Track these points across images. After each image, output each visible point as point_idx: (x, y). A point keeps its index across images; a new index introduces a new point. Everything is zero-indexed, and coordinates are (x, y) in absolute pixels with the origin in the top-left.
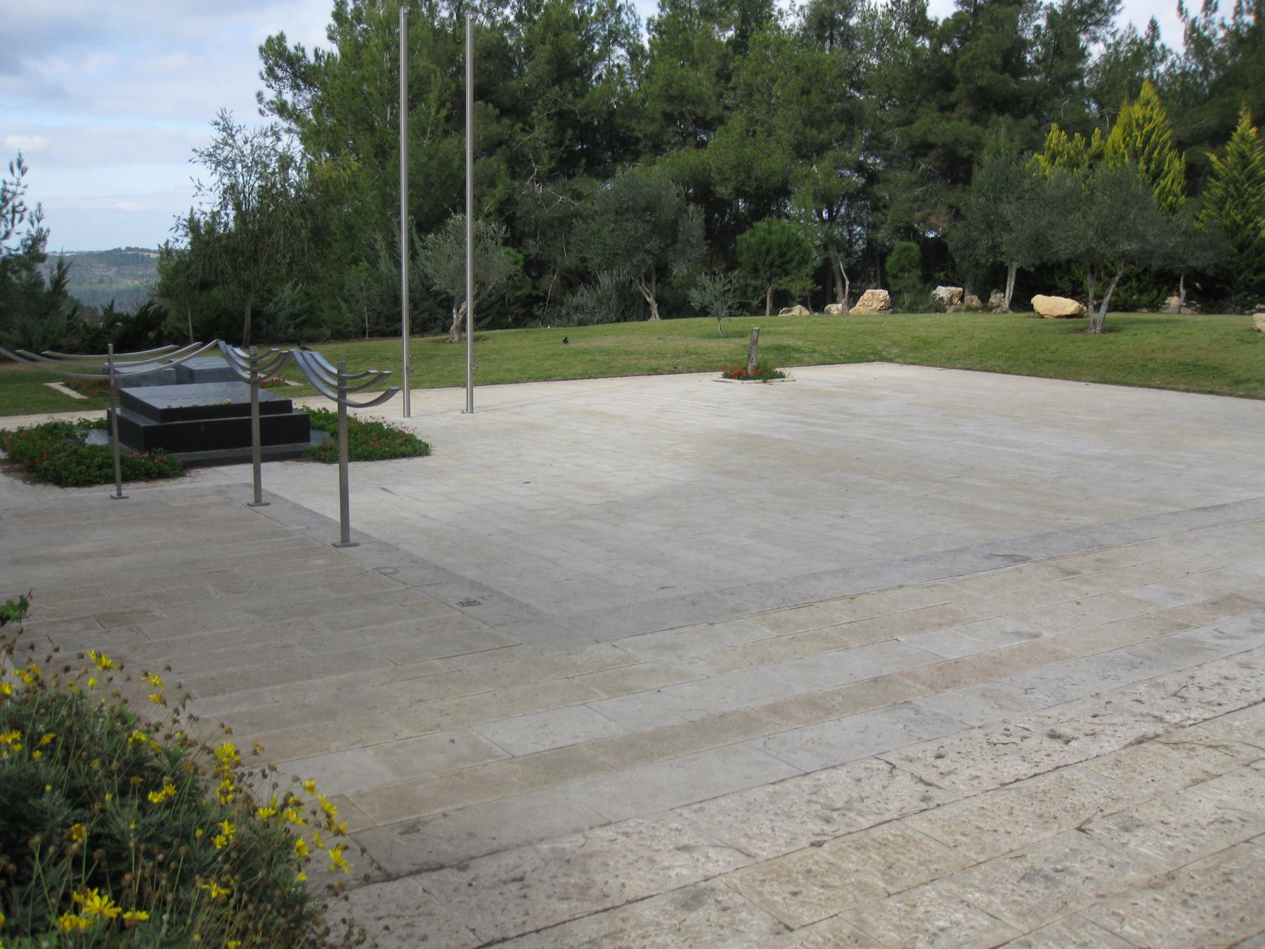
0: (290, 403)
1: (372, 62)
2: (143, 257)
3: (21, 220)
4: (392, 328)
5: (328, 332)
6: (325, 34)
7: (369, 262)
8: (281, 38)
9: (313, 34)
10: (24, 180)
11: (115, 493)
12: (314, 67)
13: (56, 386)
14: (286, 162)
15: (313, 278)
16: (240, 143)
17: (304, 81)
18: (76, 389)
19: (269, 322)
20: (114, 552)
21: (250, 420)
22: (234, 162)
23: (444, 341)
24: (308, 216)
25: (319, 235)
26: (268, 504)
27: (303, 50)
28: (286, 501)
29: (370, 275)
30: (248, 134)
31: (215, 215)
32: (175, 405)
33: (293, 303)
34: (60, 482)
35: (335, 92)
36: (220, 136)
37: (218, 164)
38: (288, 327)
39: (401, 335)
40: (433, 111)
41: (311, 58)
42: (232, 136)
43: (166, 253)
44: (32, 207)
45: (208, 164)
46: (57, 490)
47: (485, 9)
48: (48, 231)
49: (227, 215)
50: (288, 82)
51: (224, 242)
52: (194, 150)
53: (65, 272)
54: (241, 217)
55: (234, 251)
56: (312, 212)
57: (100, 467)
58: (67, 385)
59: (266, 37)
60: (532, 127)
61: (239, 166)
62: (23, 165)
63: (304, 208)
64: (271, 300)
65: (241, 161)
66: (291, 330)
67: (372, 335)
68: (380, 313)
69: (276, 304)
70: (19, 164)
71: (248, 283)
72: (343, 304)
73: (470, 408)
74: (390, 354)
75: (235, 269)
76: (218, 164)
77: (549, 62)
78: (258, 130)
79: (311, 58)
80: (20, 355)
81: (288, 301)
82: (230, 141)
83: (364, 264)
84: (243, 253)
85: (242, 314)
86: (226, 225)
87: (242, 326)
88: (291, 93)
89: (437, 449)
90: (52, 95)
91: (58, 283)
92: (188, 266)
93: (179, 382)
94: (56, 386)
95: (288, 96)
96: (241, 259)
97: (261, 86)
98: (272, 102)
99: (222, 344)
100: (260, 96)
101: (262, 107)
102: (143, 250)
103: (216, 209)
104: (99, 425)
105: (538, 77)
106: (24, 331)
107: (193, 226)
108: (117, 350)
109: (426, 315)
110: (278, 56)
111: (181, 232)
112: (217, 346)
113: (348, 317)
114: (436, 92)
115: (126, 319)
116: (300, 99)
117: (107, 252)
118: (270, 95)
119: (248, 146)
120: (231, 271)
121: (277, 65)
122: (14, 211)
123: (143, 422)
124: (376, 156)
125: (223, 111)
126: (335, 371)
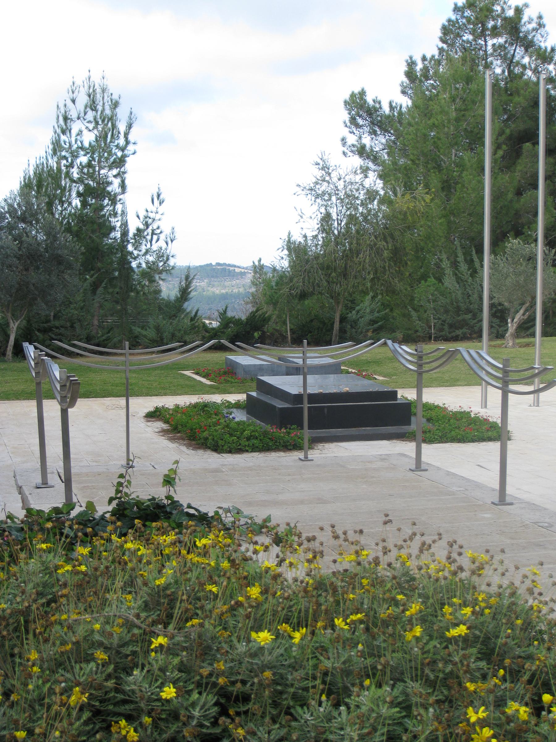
0: (395, 393)
1: (441, 112)
2: (230, 271)
3: (158, 240)
4: (453, 334)
6: (399, 89)
7: (435, 278)
8: (363, 93)
9: (389, 92)
10: (161, 209)
11: (302, 457)
12: (389, 116)
13: (188, 373)
14: (371, 195)
15: (391, 291)
16: (335, 179)
17: (380, 127)
20: (321, 501)
21: (302, 408)
24: (389, 239)
25: (397, 255)
26: (426, 470)
27: (380, 103)
28: (439, 469)
29: (437, 289)
33: (372, 311)
34: (217, 449)
35: (410, 137)
36: (320, 174)
38: (368, 331)
39: (480, 336)
41: (386, 109)
42: (329, 174)
44: (166, 228)
45: (309, 196)
46: (215, 455)
47: (533, 66)
50: (367, 129)
52: (299, 186)
53: (190, 283)
55: (328, 267)
56: (392, 236)
57: (248, 439)
58: (197, 374)
59: (350, 93)
61: (334, 198)
62: (161, 197)
63: (387, 234)
64: (353, 309)
67: (437, 339)
68: (444, 321)
69: (358, 312)
70: (159, 196)
72: (413, 313)
75: (328, 282)
78: (350, 168)
79: (386, 109)
80: (238, 347)
81: (368, 310)
82: (327, 178)
88: (369, 138)
91: (185, 293)
92: (291, 280)
93: (287, 374)
94: (188, 373)
95: (367, 140)
96: (334, 274)
97: (345, 132)
98: (353, 146)
99: (389, 342)
100: (343, 140)
101: (345, 149)
102: (229, 265)
104: (238, 405)
106: (158, 329)
108: (309, 344)
110: (360, 109)
112: (385, 344)
115: (238, 322)
116: (377, 143)
117: (201, 267)
118: (352, 139)
120: (325, 284)
122: (153, 234)
123: (280, 404)
124: (443, 189)
126: (501, 366)
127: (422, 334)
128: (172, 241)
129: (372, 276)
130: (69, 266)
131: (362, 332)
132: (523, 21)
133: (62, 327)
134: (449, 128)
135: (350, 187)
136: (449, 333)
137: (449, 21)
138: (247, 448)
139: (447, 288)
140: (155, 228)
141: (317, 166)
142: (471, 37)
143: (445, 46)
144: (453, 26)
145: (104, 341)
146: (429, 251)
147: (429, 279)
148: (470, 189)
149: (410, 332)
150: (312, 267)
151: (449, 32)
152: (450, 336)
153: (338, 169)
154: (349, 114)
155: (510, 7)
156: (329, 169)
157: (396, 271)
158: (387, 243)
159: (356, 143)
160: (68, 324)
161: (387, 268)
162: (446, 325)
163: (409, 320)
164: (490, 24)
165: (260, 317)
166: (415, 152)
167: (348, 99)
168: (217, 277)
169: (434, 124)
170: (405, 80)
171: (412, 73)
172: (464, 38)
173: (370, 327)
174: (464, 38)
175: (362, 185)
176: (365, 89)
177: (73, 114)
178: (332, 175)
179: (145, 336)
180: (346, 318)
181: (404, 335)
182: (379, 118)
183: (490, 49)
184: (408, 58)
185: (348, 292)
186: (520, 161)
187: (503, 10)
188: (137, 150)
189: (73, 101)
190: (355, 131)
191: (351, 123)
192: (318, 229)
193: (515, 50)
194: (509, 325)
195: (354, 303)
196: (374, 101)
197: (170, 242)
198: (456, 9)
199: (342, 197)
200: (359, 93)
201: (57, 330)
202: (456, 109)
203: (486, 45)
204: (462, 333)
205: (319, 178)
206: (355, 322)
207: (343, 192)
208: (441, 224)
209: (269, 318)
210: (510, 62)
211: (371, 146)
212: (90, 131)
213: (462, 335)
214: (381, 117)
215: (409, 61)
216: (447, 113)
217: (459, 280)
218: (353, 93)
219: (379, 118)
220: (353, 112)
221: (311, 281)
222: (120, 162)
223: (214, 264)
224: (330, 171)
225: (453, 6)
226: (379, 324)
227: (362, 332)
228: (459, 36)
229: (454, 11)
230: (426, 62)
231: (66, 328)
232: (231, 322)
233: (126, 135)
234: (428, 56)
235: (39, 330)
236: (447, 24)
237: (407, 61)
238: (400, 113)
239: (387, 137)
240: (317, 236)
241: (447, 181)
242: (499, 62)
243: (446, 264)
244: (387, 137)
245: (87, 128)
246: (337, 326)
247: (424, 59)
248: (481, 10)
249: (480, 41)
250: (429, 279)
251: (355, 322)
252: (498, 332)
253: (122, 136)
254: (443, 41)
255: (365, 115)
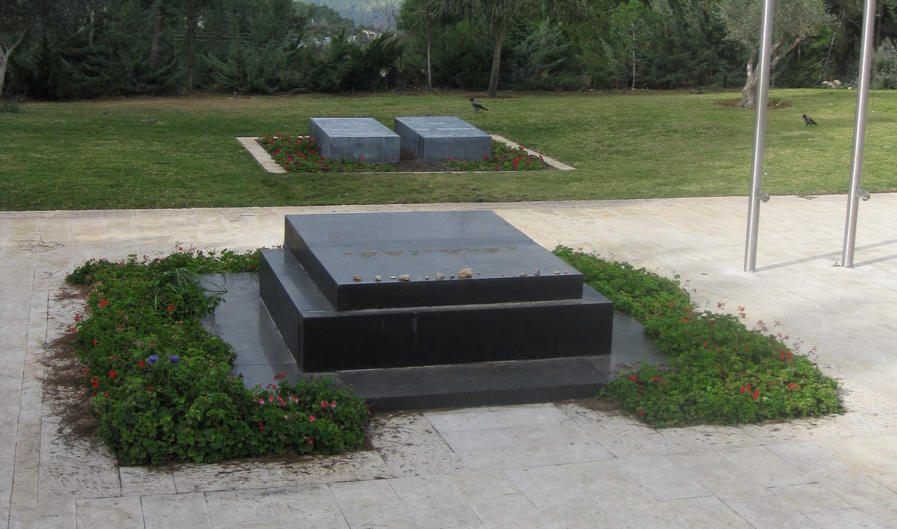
4: (663, 79)
5: (587, 79)
18: (273, 151)
19: (519, 64)
29: (642, 16)
32: (367, 279)
33: (549, 43)
38: (542, 71)
66: (545, 75)
67: (639, 86)
68: (651, 61)
69: (530, 43)
71: (500, 20)
72: (607, 48)
73: (849, 254)
74: (675, 124)
81: (543, 41)
85: (490, 54)
87: (489, 69)
89: (856, 391)
109: (704, 66)
113: (613, 64)
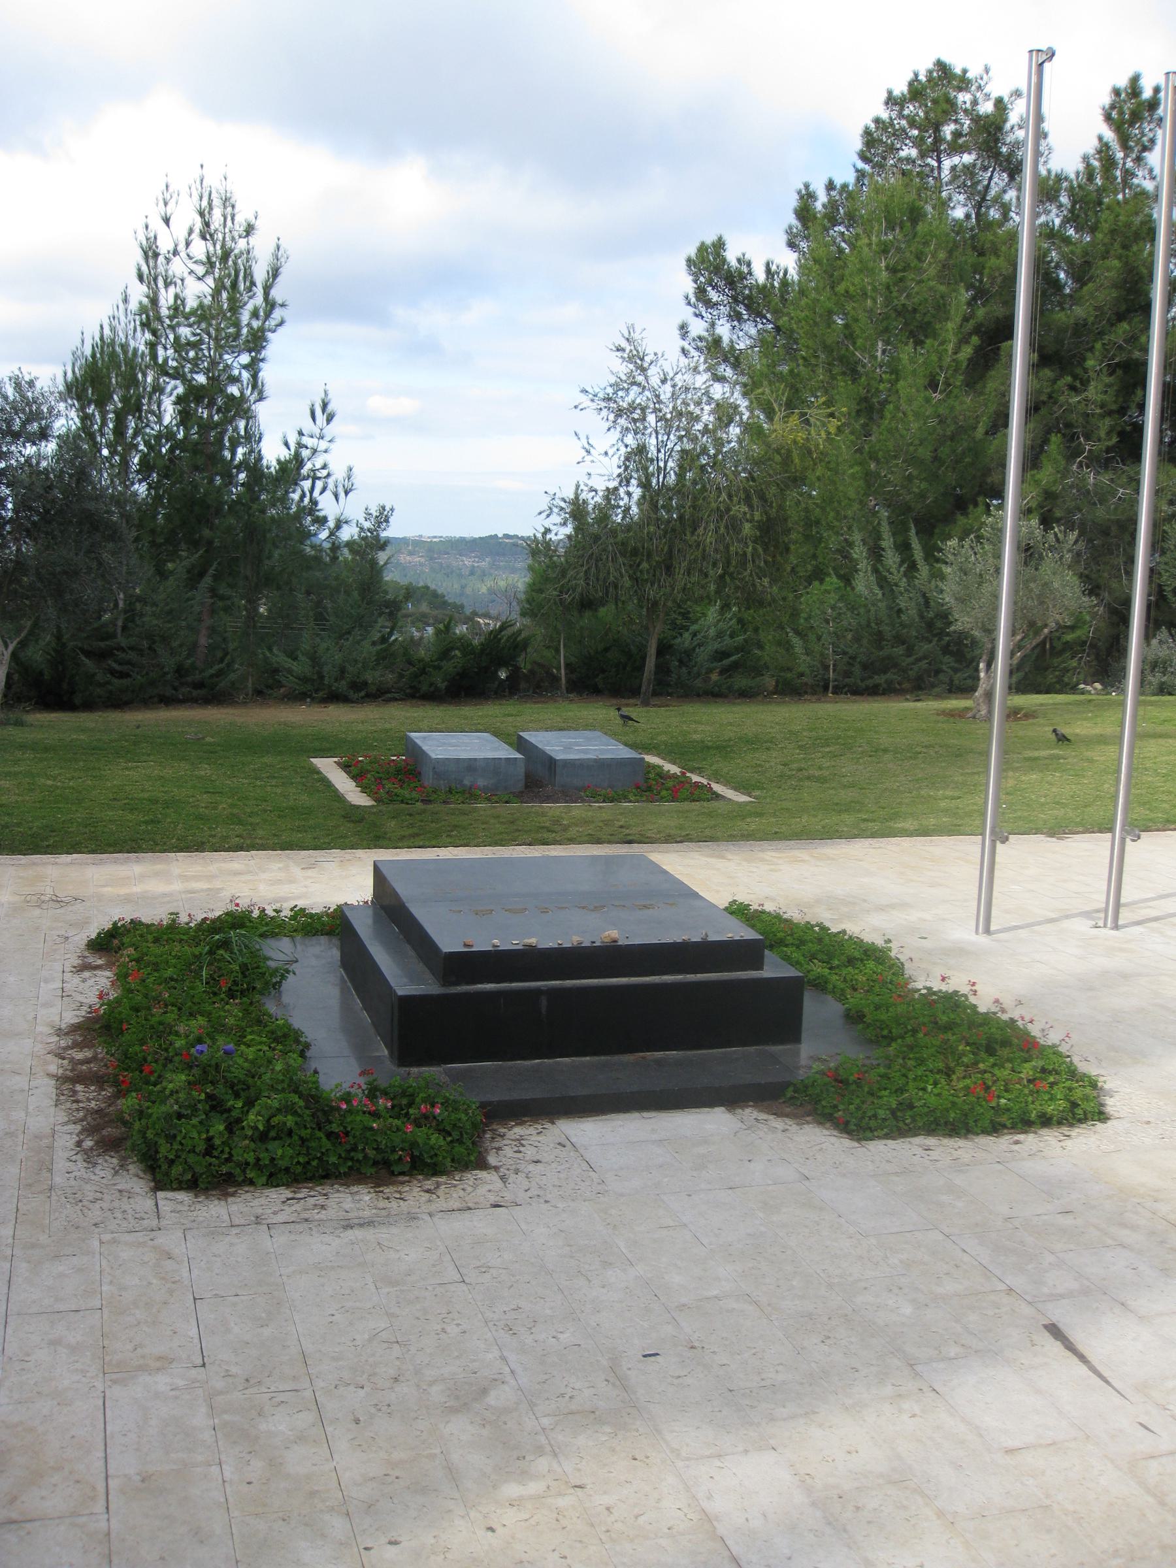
1: (860, 271)
4: (870, 682)
5: (769, 682)
6: (784, 238)
7: (839, 577)
9: (766, 248)
10: (330, 431)
15: (753, 600)
16: (655, 381)
17: (748, 308)
18: (358, 776)
22: (643, 409)
23: (960, 714)
24: (755, 501)
25: (770, 532)
27: (749, 264)
29: (841, 598)
30: (668, 369)
31: (611, 493)
33: (720, 635)
36: (623, 369)
37: (620, 412)
38: (710, 671)
40: (950, 347)
41: (760, 276)
42: (643, 370)
43: (539, 548)
44: (338, 472)
45: (605, 413)
48: (392, 510)
49: (629, 494)
50: (724, 310)
51: (621, 536)
52: (584, 391)
54: (651, 497)
55: (635, 552)
56: (763, 498)
60: (1085, 383)
61: (651, 419)
62: (330, 408)
63: (752, 494)
65: (655, 411)
66: (714, 677)
67: (837, 690)
68: (853, 658)
69: (695, 634)
70: (325, 406)
71: (655, 604)
72: (796, 641)
73: (1113, 912)
76: (620, 412)
77: (1115, 286)
79: (760, 276)
81: (712, 632)
82: (640, 379)
83: (832, 581)
84: (649, 555)
86: (627, 509)
87: (641, 668)
88: (728, 326)
89: (1123, 1092)
90: (424, 350)
95: (724, 330)
96: (645, 565)
98: (700, 338)
103: (612, 485)
105: (1096, 308)
107: (577, 510)
109: (923, 664)
110: (713, 269)
111: (556, 518)
113: (803, 662)
114: (958, 320)
116: (741, 336)
118: (698, 328)
119: (668, 388)
121: (710, 282)
125: (631, 328)
127: (810, 681)
128: (347, 493)
129: (720, 571)
130: (114, 535)
131: (699, 674)
132: (1008, 126)
133: (132, 648)
134: (874, 300)
135: (683, 396)
136: (862, 680)
137: (877, 121)
138: (250, 1174)
139: (860, 596)
140: (318, 466)
141: (619, 354)
142: (914, 153)
143: (867, 168)
144: (885, 129)
145: (212, 676)
146: (830, 527)
147: (828, 579)
148: (910, 413)
149: (789, 675)
150: (604, 550)
151: (876, 143)
152: (863, 685)
153: (661, 362)
154: (695, 281)
155: (987, 96)
156: (642, 360)
157: (766, 562)
158: (751, 507)
159: (705, 334)
160: (145, 643)
161: (749, 557)
162: (858, 666)
163: (788, 650)
164: (948, 130)
165: (507, 640)
166: (810, 343)
167: (693, 256)
168: (504, 555)
169: (847, 292)
170: (795, 222)
171: (808, 211)
172: (903, 154)
173: (715, 664)
174: (903, 154)
175: (707, 393)
176: (725, 238)
177: (165, 246)
178: (650, 373)
179: (290, 671)
180: (671, 646)
181: (777, 682)
182: (747, 292)
183: (946, 174)
184: (802, 187)
185: (674, 601)
186: (993, 373)
187: (975, 102)
188: (286, 318)
189: (167, 221)
190: (704, 314)
191: (698, 299)
192: (619, 475)
193: (991, 178)
194: (982, 675)
195: (688, 618)
196: (739, 260)
197: (342, 495)
198: (891, 101)
199: (669, 416)
200: (714, 245)
201: (123, 655)
202: (887, 268)
203: (939, 167)
204: (886, 681)
205: (624, 378)
206: (689, 653)
207: (671, 406)
208: (853, 476)
209: (525, 644)
210: (980, 200)
211: (731, 341)
212: (199, 279)
213: (885, 686)
214: (750, 290)
215: (804, 192)
216: (871, 272)
217: (882, 582)
218: (703, 244)
219: (747, 292)
220: (702, 279)
221: (601, 576)
222: (257, 342)
223: (500, 535)
224: (646, 365)
225: (885, 95)
226: (733, 658)
227: (699, 674)
228: (892, 149)
229: (887, 103)
230: (833, 193)
231: (142, 650)
232: (452, 649)
233: (267, 289)
234: (838, 182)
235: (88, 654)
236: (873, 126)
237: (799, 192)
238: (785, 283)
239: (760, 326)
240: (616, 489)
241: (866, 399)
242: (962, 198)
243: (859, 552)
244: (760, 326)
245: (192, 272)
246: (651, 663)
247: (830, 186)
248: (935, 102)
249: (929, 160)
250: (828, 579)
251: (689, 653)
252: (951, 681)
253: (259, 291)
254: (863, 157)
255: (722, 284)
